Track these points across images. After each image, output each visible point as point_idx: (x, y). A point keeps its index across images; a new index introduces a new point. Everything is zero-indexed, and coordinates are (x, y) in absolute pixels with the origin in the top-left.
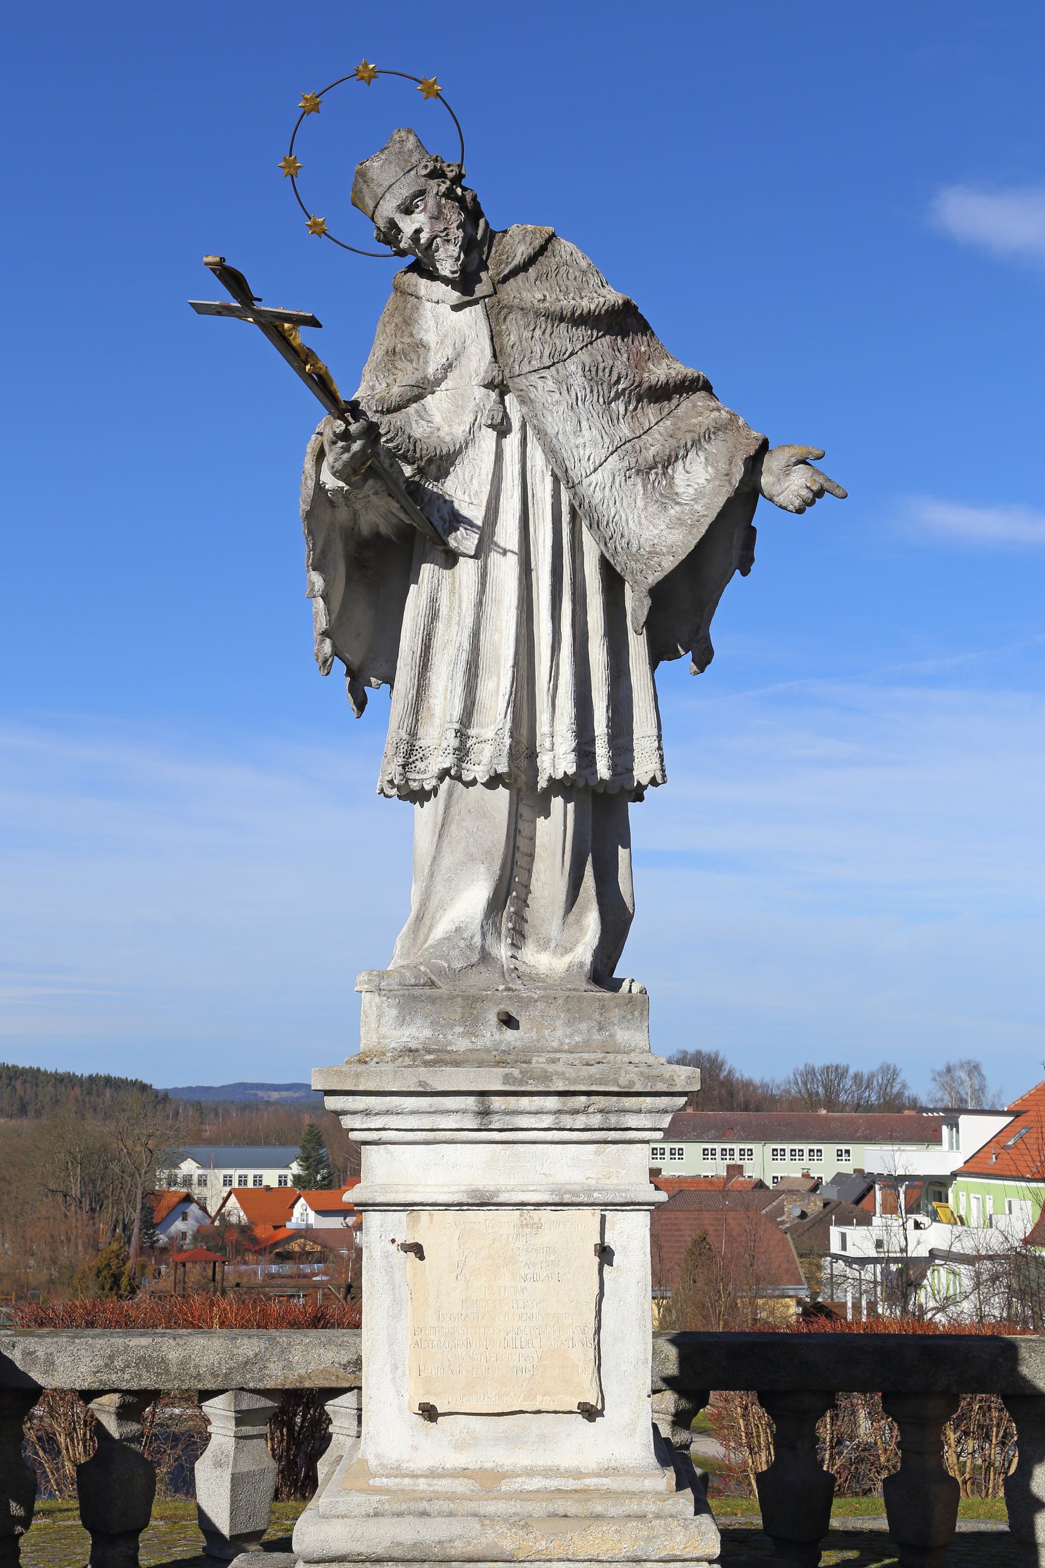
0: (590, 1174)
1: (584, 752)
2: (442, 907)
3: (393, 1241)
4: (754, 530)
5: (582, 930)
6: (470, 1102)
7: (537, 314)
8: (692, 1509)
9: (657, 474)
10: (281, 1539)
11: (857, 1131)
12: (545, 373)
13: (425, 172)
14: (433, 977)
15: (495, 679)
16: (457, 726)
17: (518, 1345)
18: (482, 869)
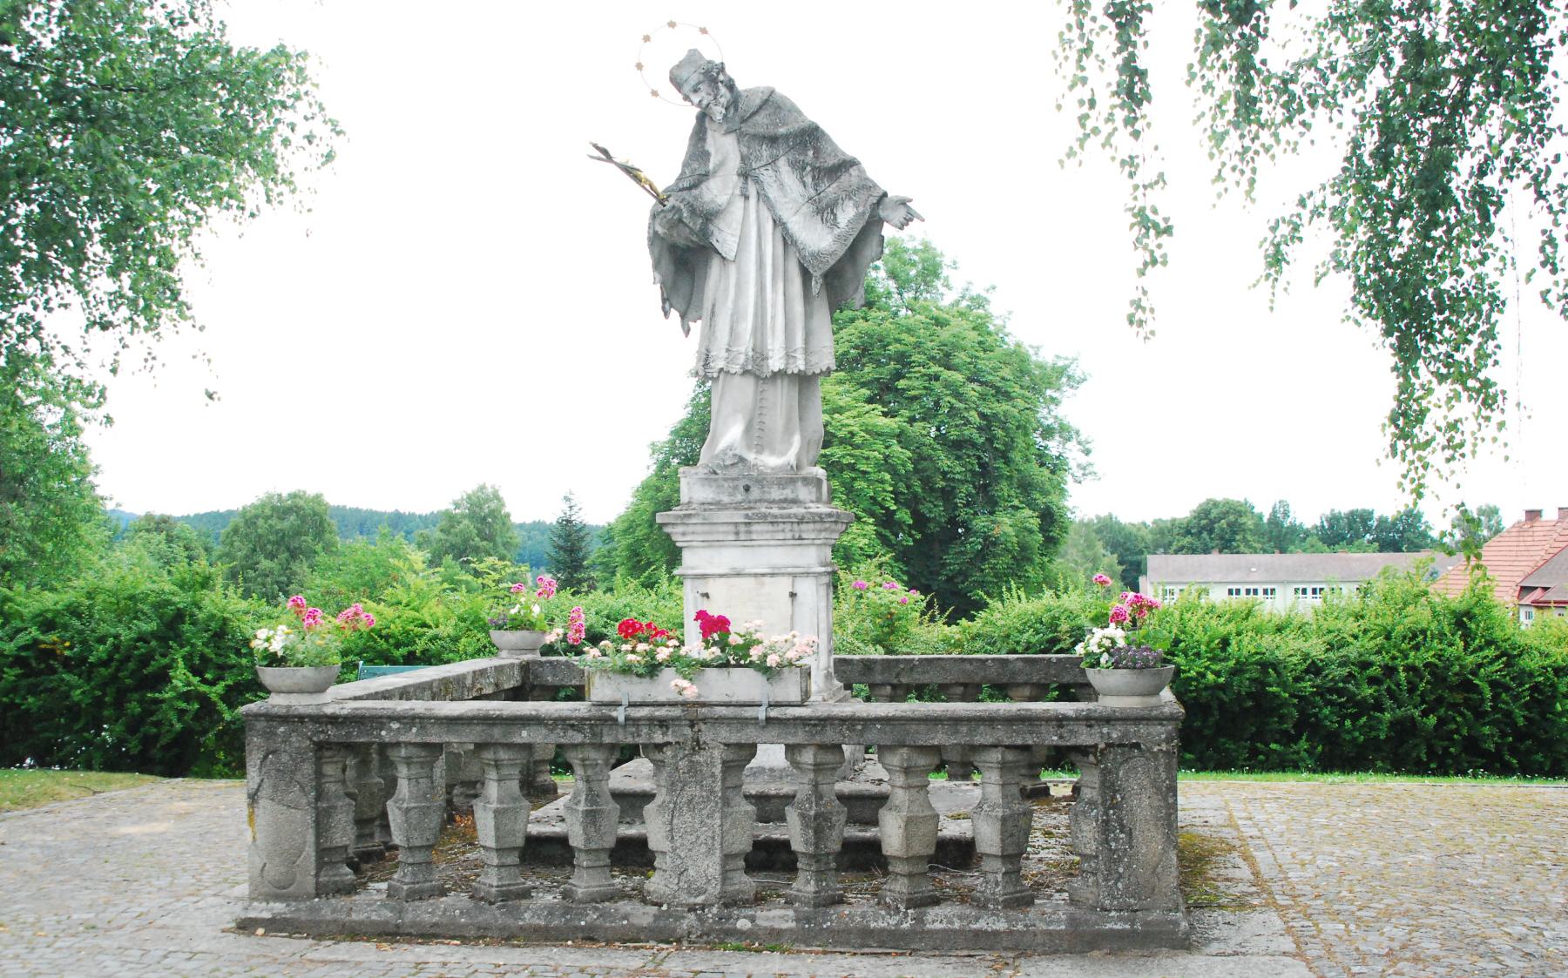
1: (789, 356)
5: (791, 444)
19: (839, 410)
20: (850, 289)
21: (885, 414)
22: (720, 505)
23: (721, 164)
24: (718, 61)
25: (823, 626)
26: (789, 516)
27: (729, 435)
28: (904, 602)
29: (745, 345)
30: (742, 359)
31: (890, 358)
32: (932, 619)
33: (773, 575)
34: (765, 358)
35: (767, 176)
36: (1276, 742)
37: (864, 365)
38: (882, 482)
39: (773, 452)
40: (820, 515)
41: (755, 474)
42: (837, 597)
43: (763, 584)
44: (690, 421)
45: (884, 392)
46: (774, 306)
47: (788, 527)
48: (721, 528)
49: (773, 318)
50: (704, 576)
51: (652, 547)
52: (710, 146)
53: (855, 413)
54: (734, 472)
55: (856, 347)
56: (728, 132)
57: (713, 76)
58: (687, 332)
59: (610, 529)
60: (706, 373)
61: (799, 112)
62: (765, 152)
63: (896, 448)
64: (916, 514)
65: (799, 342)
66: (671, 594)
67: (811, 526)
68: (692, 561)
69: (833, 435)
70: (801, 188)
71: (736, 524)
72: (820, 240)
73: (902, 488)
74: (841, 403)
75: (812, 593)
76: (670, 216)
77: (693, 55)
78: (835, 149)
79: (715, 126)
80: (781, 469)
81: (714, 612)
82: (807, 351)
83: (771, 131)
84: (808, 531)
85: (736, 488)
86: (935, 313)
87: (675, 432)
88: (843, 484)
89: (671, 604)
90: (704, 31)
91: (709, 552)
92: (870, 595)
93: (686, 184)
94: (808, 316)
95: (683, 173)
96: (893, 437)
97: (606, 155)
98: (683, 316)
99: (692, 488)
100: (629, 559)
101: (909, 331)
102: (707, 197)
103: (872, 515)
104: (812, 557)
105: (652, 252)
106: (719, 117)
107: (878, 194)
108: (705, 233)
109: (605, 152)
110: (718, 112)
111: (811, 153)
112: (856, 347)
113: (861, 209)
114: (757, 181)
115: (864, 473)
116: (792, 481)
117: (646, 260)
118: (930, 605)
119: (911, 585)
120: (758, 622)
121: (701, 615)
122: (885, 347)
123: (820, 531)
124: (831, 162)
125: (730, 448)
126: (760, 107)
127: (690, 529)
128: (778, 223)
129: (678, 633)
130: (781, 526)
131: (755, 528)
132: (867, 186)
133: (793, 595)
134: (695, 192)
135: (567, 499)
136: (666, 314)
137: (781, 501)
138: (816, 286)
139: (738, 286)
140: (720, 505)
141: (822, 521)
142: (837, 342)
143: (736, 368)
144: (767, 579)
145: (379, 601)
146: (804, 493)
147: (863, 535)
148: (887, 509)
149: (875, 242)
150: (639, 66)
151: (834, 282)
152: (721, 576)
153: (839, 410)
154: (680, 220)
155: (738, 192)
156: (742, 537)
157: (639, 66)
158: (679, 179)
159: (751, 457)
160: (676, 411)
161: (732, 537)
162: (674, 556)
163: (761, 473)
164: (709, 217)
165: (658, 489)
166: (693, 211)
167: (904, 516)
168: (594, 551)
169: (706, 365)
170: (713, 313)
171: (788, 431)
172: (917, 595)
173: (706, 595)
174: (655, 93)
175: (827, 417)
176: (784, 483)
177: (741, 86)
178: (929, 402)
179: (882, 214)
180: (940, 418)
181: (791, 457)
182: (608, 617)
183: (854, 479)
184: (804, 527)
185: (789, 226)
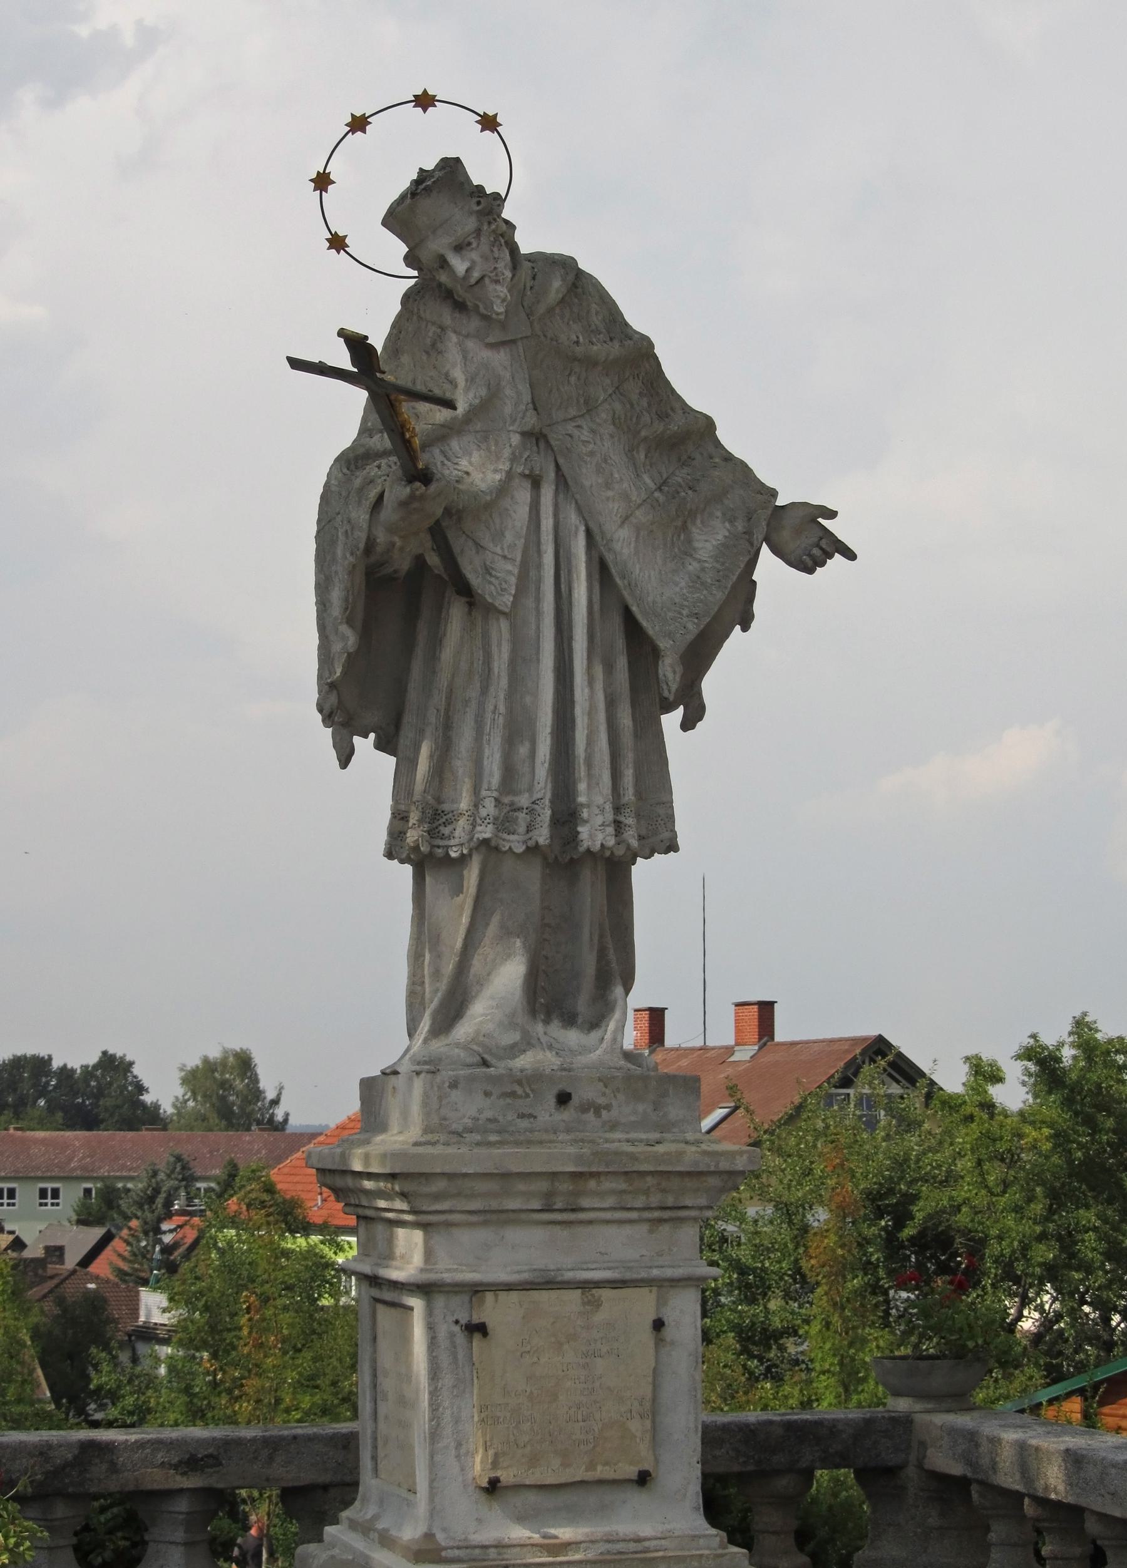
0: (644, 1252)
2: (481, 982)
3: (457, 1322)
4: (755, 582)
6: (543, 1185)
10: (1017, 1492)
11: (71, 1160)
12: (579, 422)
14: (486, 1056)
15: (527, 744)
17: (580, 1418)
18: (518, 943)
36: (916, 1259)
42: (453, 1133)
43: (597, 1304)
46: (591, 713)
144: (605, 1294)
145: (248, 1210)
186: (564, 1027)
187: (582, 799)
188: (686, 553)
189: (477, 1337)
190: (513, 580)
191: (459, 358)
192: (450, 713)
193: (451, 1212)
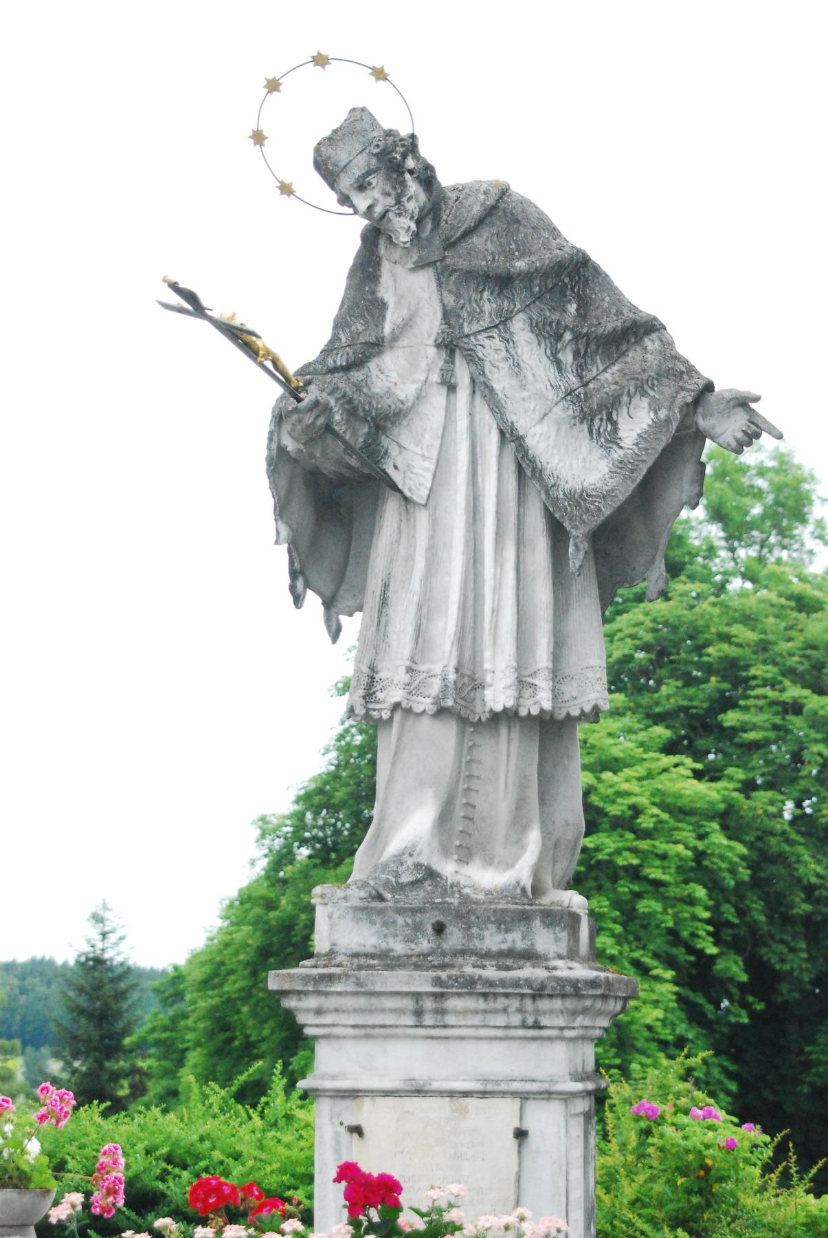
1: (523, 684)
5: (523, 848)
7: (320, 437)
8: (335, 1175)
9: (601, 420)
13: (377, 150)
16: (408, 663)
19: (613, 765)
20: (640, 561)
21: (698, 775)
22: (388, 960)
23: (406, 325)
24: (404, 132)
25: (577, 1195)
26: (516, 983)
27: (407, 825)
28: (731, 1146)
29: (442, 660)
30: (435, 687)
31: (709, 670)
32: (785, 1182)
33: (484, 1094)
34: (478, 685)
35: (490, 349)
37: (659, 683)
38: (691, 901)
39: (489, 861)
40: (575, 983)
41: (455, 901)
43: (465, 1112)
44: (334, 777)
45: (696, 733)
46: (497, 589)
47: (515, 1004)
48: (389, 1003)
49: (496, 612)
50: (354, 1094)
51: (254, 1014)
52: (386, 291)
53: (640, 770)
54: (416, 898)
55: (646, 648)
56: (420, 266)
57: (396, 159)
58: (335, 633)
59: (178, 977)
60: (369, 729)
61: (555, 233)
62: (488, 305)
63: (719, 838)
64: (754, 965)
65: (542, 657)
66: (289, 1118)
67: (557, 1004)
68: (332, 1063)
69: (601, 812)
70: (552, 373)
71: (417, 996)
72: (584, 468)
73: (729, 912)
74: (616, 752)
75: (558, 1131)
76: (308, 419)
77: (359, 119)
78: (618, 298)
79: (397, 254)
80: (504, 893)
81: (372, 1166)
82: (556, 675)
83: (500, 265)
84: (553, 1013)
85: (418, 927)
86: (797, 586)
87: (306, 799)
88: (617, 904)
89: (288, 1138)
90: (380, 74)
91: (366, 1047)
92: (669, 1131)
93: (341, 361)
94: (560, 609)
95: (335, 339)
96: (711, 818)
97: (193, 304)
98: (329, 604)
99: (337, 926)
100: (211, 1034)
101: (748, 619)
102: (378, 385)
103: (670, 963)
104: (559, 1061)
105: (274, 486)
106: (404, 238)
107: (694, 385)
108: (373, 452)
109: (191, 297)
110: (403, 228)
111: (572, 308)
112: (646, 648)
113: (663, 414)
114: (472, 358)
115: (658, 884)
116: (524, 917)
117: (263, 500)
118: (781, 1152)
119: (743, 1114)
120: (455, 1188)
121: (348, 1172)
122: (699, 649)
123: (574, 1013)
124: (610, 325)
125: (410, 851)
126: (481, 222)
127: (332, 1002)
128: (509, 436)
129: (299, 1195)
130: (501, 1003)
131: (452, 1003)
132: (676, 369)
133: (521, 1134)
134: (357, 375)
135: (98, 919)
136: (298, 600)
137: (502, 954)
138: (576, 555)
139: (432, 550)
140: (388, 960)
141: (577, 994)
142: (610, 637)
143: (424, 704)
144: (471, 1102)
146: (546, 940)
147: (656, 1003)
148: (700, 953)
149: (689, 471)
150: (258, 138)
151: (611, 545)
152: (387, 1093)
153: (613, 765)
154: (328, 428)
155: (435, 377)
156: (428, 1020)
157: (258, 138)
158: (327, 351)
159: (448, 869)
160: (312, 760)
161: (409, 1020)
162: (294, 1042)
163: (466, 900)
164: (382, 421)
165: (270, 905)
166: (352, 411)
167: (733, 967)
168: (147, 1018)
169: (369, 696)
170: (384, 601)
171: (519, 824)
172: (753, 1134)
173: (357, 1130)
174: (286, 189)
175: (587, 778)
176: (504, 921)
177: (446, 178)
178: (780, 753)
179: (703, 423)
180: (803, 784)
181: (521, 872)
182: (169, 1159)
183: (638, 896)
184: (544, 1004)
185: (529, 442)
186: (484, 867)
187: (487, 666)
188: (611, 442)
189: (355, 1135)
190: (429, 476)
191: (391, 283)
192: (390, 594)
193: (334, 1025)
